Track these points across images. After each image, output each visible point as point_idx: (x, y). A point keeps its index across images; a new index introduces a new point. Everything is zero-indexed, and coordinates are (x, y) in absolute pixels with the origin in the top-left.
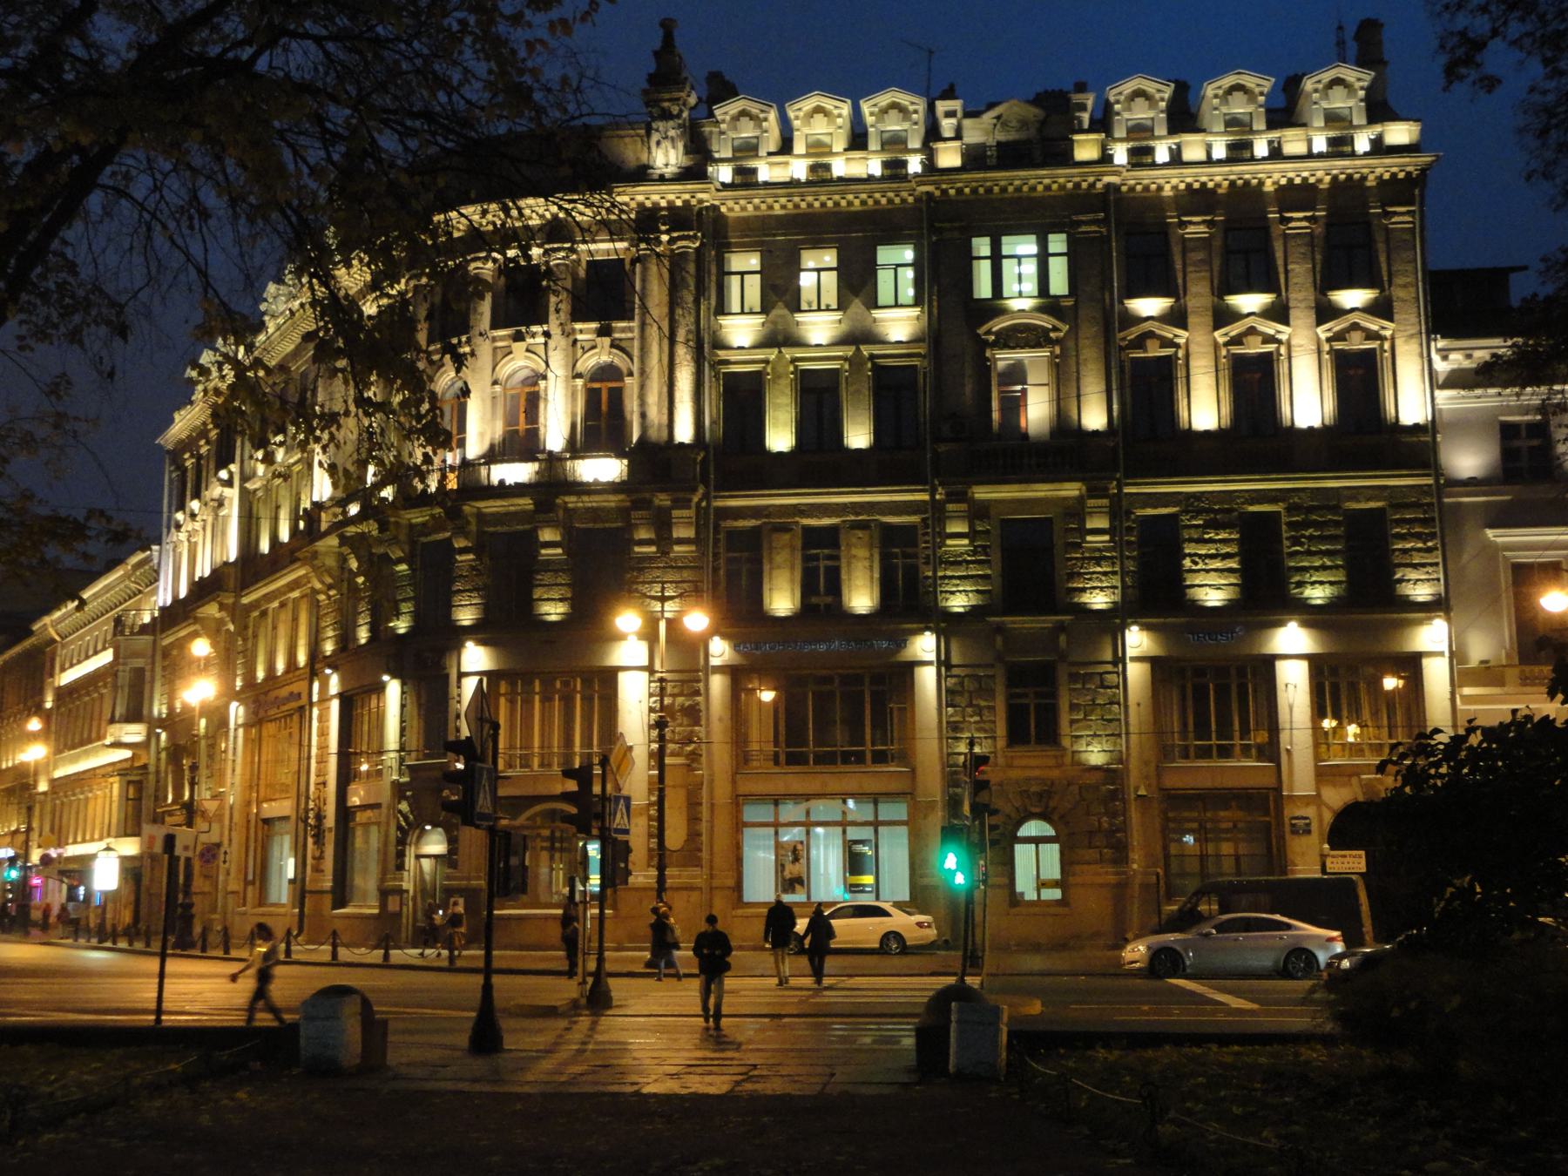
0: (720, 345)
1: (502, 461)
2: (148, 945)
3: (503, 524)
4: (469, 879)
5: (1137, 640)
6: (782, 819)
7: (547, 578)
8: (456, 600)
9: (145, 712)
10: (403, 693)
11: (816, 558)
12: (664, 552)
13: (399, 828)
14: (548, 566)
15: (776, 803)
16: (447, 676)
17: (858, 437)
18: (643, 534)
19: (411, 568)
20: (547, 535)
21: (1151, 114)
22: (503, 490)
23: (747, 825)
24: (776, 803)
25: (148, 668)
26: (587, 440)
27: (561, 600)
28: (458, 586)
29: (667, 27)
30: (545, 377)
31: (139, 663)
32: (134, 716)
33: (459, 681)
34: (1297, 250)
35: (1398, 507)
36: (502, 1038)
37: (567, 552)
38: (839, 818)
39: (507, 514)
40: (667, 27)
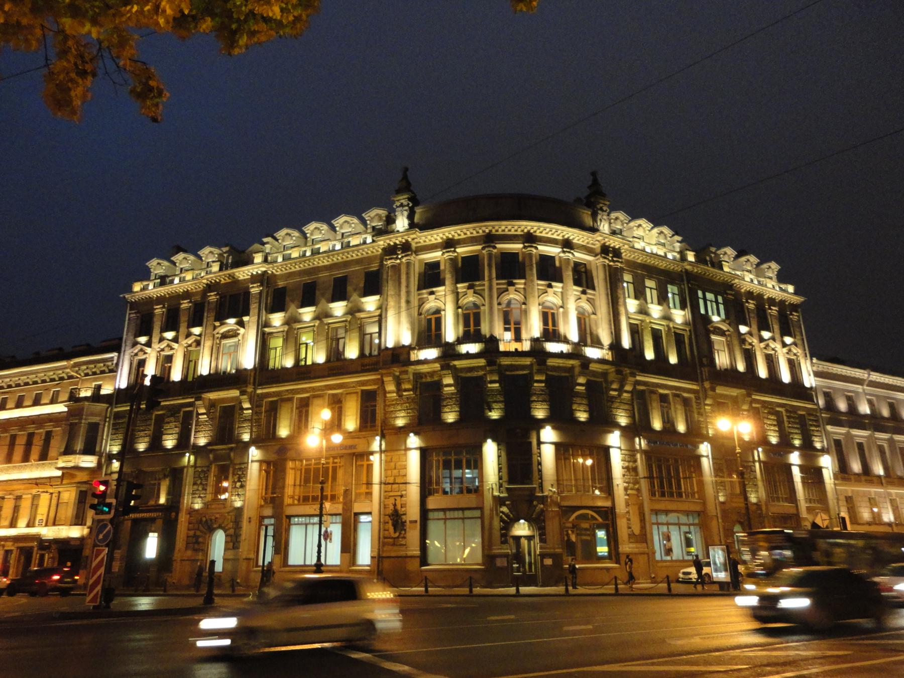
0: (360, 310)
1: (466, 343)
2: (197, 591)
3: (555, 371)
4: (554, 549)
5: (254, 453)
6: (660, 521)
7: (578, 400)
8: (533, 405)
9: (97, 449)
10: (499, 449)
11: (367, 407)
12: (620, 395)
13: (502, 520)
14: (578, 394)
15: (656, 514)
16: (530, 443)
17: (673, 359)
18: (614, 386)
19: (500, 386)
20: (582, 380)
21: (257, 267)
22: (468, 356)
23: (445, 523)
24: (656, 514)
25: (102, 423)
26: (466, 338)
27: (585, 411)
28: (534, 398)
29: (594, 174)
30: (444, 310)
31: (95, 419)
32: (89, 450)
33: (539, 448)
34: (774, 321)
35: (810, 415)
36: (824, 639)
37: (456, 388)
38: (677, 522)
39: (559, 367)
40: (594, 174)
